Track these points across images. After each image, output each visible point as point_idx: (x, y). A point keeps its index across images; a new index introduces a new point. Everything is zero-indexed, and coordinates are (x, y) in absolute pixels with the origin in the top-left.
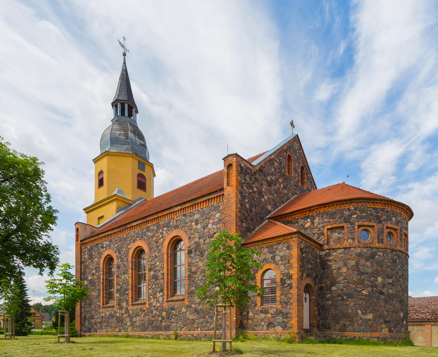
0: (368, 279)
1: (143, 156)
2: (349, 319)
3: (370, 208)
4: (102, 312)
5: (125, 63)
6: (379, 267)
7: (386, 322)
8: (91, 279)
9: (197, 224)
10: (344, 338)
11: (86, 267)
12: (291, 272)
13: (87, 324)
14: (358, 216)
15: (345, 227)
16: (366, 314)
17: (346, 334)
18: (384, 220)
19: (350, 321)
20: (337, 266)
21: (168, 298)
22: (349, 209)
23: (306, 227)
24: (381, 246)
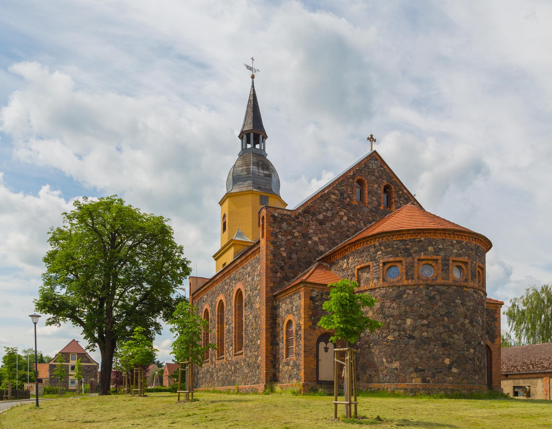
1: (267, 187)
3: (397, 240)
5: (253, 87)
6: (408, 308)
7: (417, 370)
10: (369, 390)
16: (391, 362)
17: (371, 385)
18: (414, 252)
19: (375, 371)
21: (235, 352)
22: (374, 245)
23: (344, 268)
24: (410, 283)
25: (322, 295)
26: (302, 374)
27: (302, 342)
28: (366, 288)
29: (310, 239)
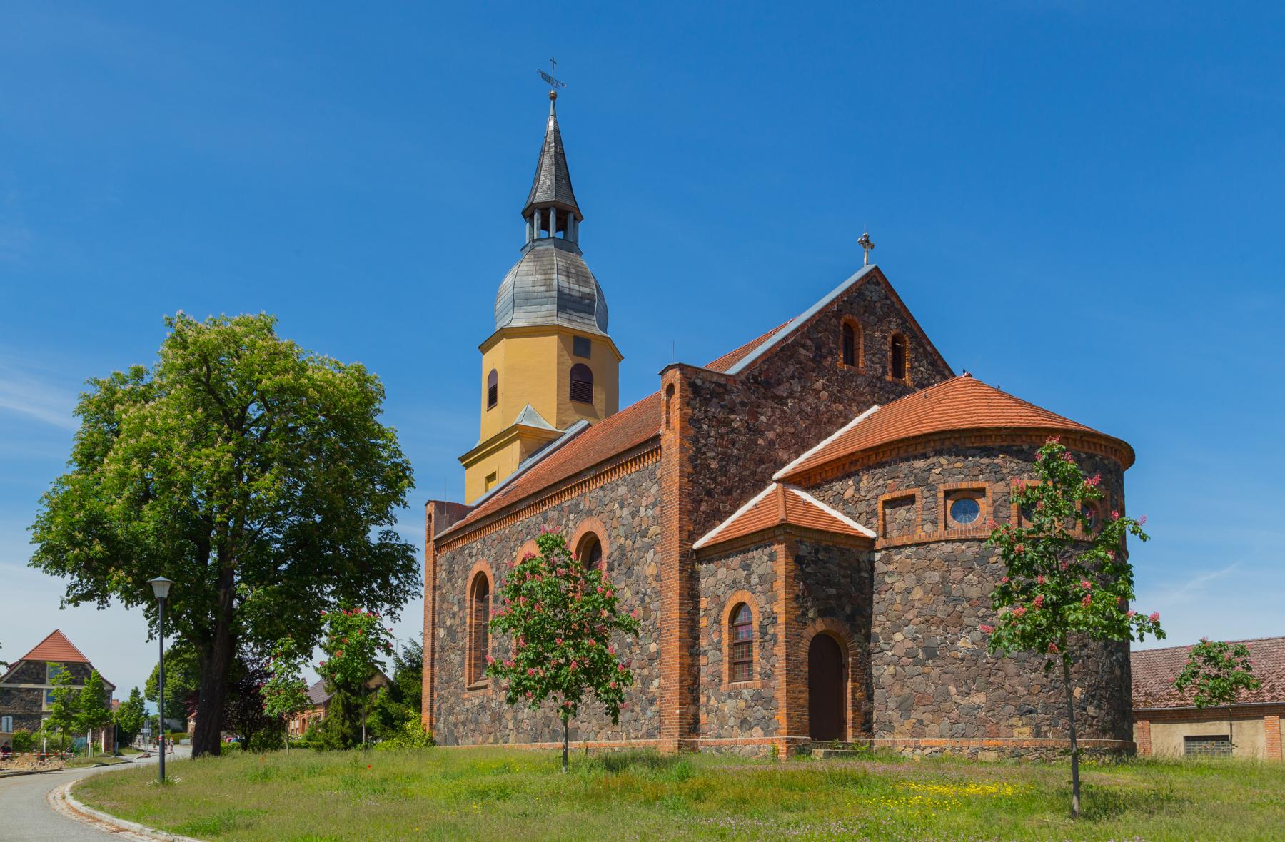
0: (972, 612)
2: (930, 708)
4: (468, 700)
8: (452, 626)
9: (621, 508)
11: (444, 600)
12: (776, 609)
13: (441, 726)
14: (944, 470)
15: (918, 498)
16: (968, 694)
20: (904, 586)
23: (846, 497)
25: (817, 552)
26: (781, 717)
27: (781, 650)
28: (905, 540)
29: (762, 433)
